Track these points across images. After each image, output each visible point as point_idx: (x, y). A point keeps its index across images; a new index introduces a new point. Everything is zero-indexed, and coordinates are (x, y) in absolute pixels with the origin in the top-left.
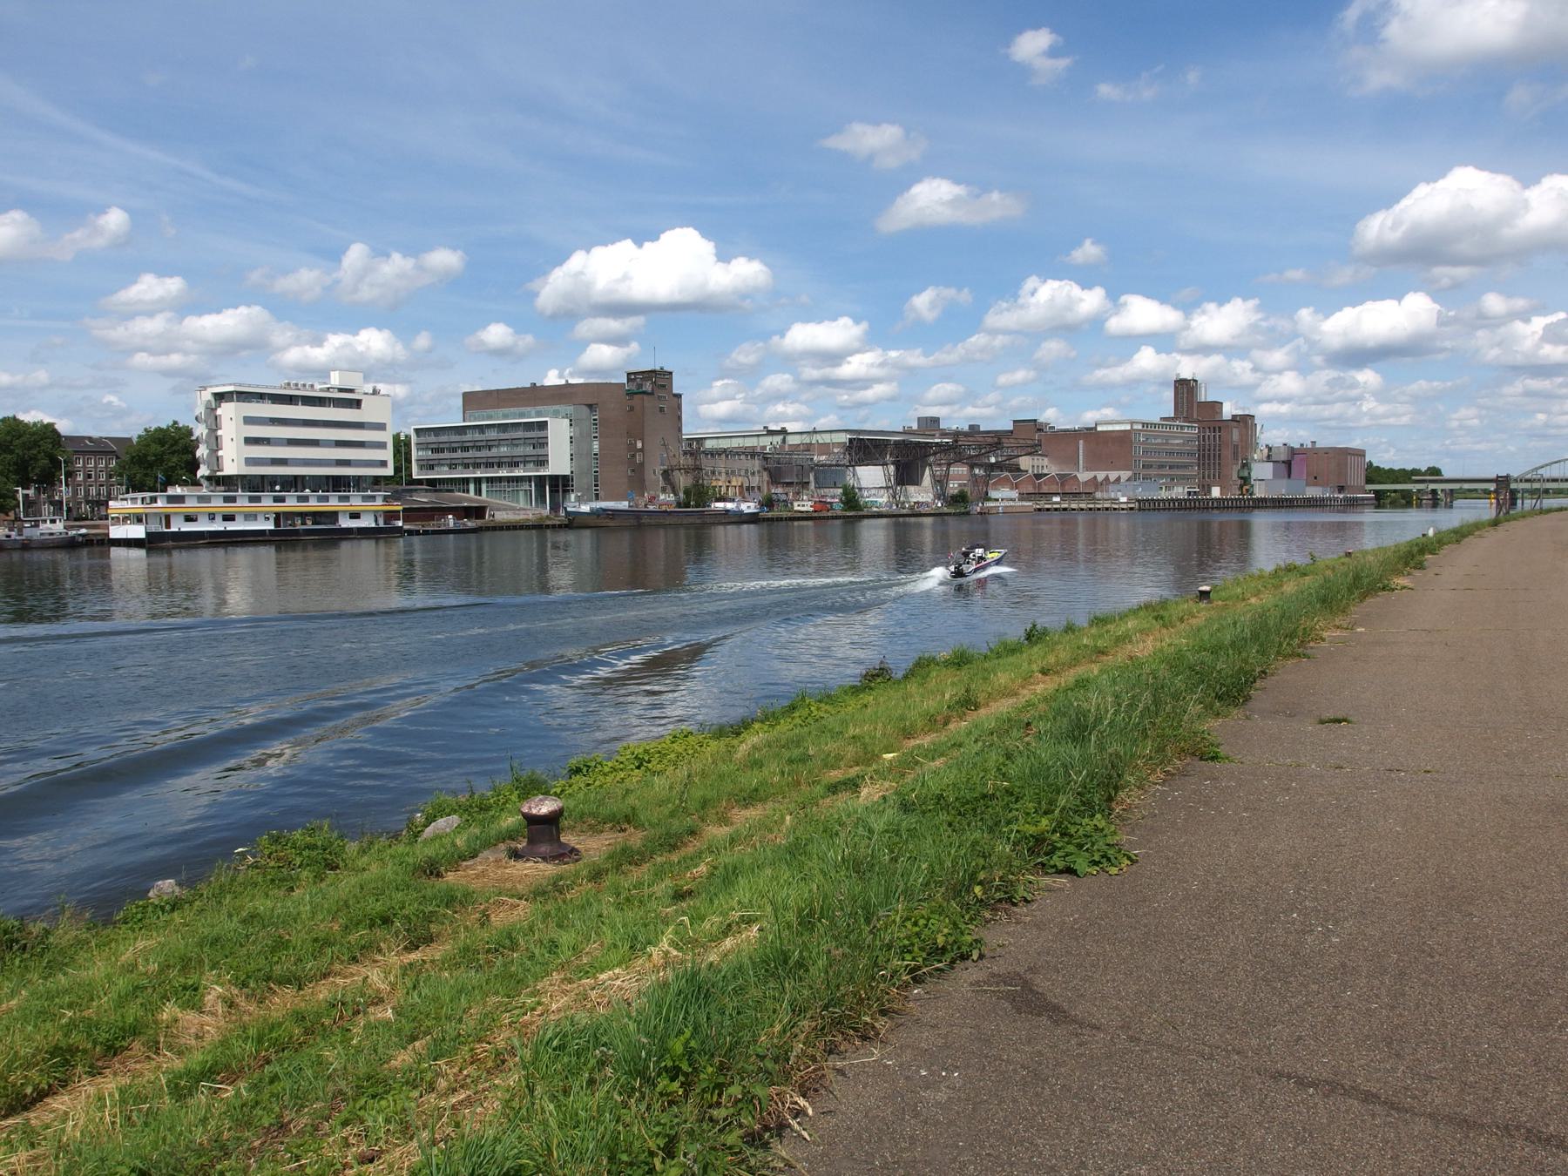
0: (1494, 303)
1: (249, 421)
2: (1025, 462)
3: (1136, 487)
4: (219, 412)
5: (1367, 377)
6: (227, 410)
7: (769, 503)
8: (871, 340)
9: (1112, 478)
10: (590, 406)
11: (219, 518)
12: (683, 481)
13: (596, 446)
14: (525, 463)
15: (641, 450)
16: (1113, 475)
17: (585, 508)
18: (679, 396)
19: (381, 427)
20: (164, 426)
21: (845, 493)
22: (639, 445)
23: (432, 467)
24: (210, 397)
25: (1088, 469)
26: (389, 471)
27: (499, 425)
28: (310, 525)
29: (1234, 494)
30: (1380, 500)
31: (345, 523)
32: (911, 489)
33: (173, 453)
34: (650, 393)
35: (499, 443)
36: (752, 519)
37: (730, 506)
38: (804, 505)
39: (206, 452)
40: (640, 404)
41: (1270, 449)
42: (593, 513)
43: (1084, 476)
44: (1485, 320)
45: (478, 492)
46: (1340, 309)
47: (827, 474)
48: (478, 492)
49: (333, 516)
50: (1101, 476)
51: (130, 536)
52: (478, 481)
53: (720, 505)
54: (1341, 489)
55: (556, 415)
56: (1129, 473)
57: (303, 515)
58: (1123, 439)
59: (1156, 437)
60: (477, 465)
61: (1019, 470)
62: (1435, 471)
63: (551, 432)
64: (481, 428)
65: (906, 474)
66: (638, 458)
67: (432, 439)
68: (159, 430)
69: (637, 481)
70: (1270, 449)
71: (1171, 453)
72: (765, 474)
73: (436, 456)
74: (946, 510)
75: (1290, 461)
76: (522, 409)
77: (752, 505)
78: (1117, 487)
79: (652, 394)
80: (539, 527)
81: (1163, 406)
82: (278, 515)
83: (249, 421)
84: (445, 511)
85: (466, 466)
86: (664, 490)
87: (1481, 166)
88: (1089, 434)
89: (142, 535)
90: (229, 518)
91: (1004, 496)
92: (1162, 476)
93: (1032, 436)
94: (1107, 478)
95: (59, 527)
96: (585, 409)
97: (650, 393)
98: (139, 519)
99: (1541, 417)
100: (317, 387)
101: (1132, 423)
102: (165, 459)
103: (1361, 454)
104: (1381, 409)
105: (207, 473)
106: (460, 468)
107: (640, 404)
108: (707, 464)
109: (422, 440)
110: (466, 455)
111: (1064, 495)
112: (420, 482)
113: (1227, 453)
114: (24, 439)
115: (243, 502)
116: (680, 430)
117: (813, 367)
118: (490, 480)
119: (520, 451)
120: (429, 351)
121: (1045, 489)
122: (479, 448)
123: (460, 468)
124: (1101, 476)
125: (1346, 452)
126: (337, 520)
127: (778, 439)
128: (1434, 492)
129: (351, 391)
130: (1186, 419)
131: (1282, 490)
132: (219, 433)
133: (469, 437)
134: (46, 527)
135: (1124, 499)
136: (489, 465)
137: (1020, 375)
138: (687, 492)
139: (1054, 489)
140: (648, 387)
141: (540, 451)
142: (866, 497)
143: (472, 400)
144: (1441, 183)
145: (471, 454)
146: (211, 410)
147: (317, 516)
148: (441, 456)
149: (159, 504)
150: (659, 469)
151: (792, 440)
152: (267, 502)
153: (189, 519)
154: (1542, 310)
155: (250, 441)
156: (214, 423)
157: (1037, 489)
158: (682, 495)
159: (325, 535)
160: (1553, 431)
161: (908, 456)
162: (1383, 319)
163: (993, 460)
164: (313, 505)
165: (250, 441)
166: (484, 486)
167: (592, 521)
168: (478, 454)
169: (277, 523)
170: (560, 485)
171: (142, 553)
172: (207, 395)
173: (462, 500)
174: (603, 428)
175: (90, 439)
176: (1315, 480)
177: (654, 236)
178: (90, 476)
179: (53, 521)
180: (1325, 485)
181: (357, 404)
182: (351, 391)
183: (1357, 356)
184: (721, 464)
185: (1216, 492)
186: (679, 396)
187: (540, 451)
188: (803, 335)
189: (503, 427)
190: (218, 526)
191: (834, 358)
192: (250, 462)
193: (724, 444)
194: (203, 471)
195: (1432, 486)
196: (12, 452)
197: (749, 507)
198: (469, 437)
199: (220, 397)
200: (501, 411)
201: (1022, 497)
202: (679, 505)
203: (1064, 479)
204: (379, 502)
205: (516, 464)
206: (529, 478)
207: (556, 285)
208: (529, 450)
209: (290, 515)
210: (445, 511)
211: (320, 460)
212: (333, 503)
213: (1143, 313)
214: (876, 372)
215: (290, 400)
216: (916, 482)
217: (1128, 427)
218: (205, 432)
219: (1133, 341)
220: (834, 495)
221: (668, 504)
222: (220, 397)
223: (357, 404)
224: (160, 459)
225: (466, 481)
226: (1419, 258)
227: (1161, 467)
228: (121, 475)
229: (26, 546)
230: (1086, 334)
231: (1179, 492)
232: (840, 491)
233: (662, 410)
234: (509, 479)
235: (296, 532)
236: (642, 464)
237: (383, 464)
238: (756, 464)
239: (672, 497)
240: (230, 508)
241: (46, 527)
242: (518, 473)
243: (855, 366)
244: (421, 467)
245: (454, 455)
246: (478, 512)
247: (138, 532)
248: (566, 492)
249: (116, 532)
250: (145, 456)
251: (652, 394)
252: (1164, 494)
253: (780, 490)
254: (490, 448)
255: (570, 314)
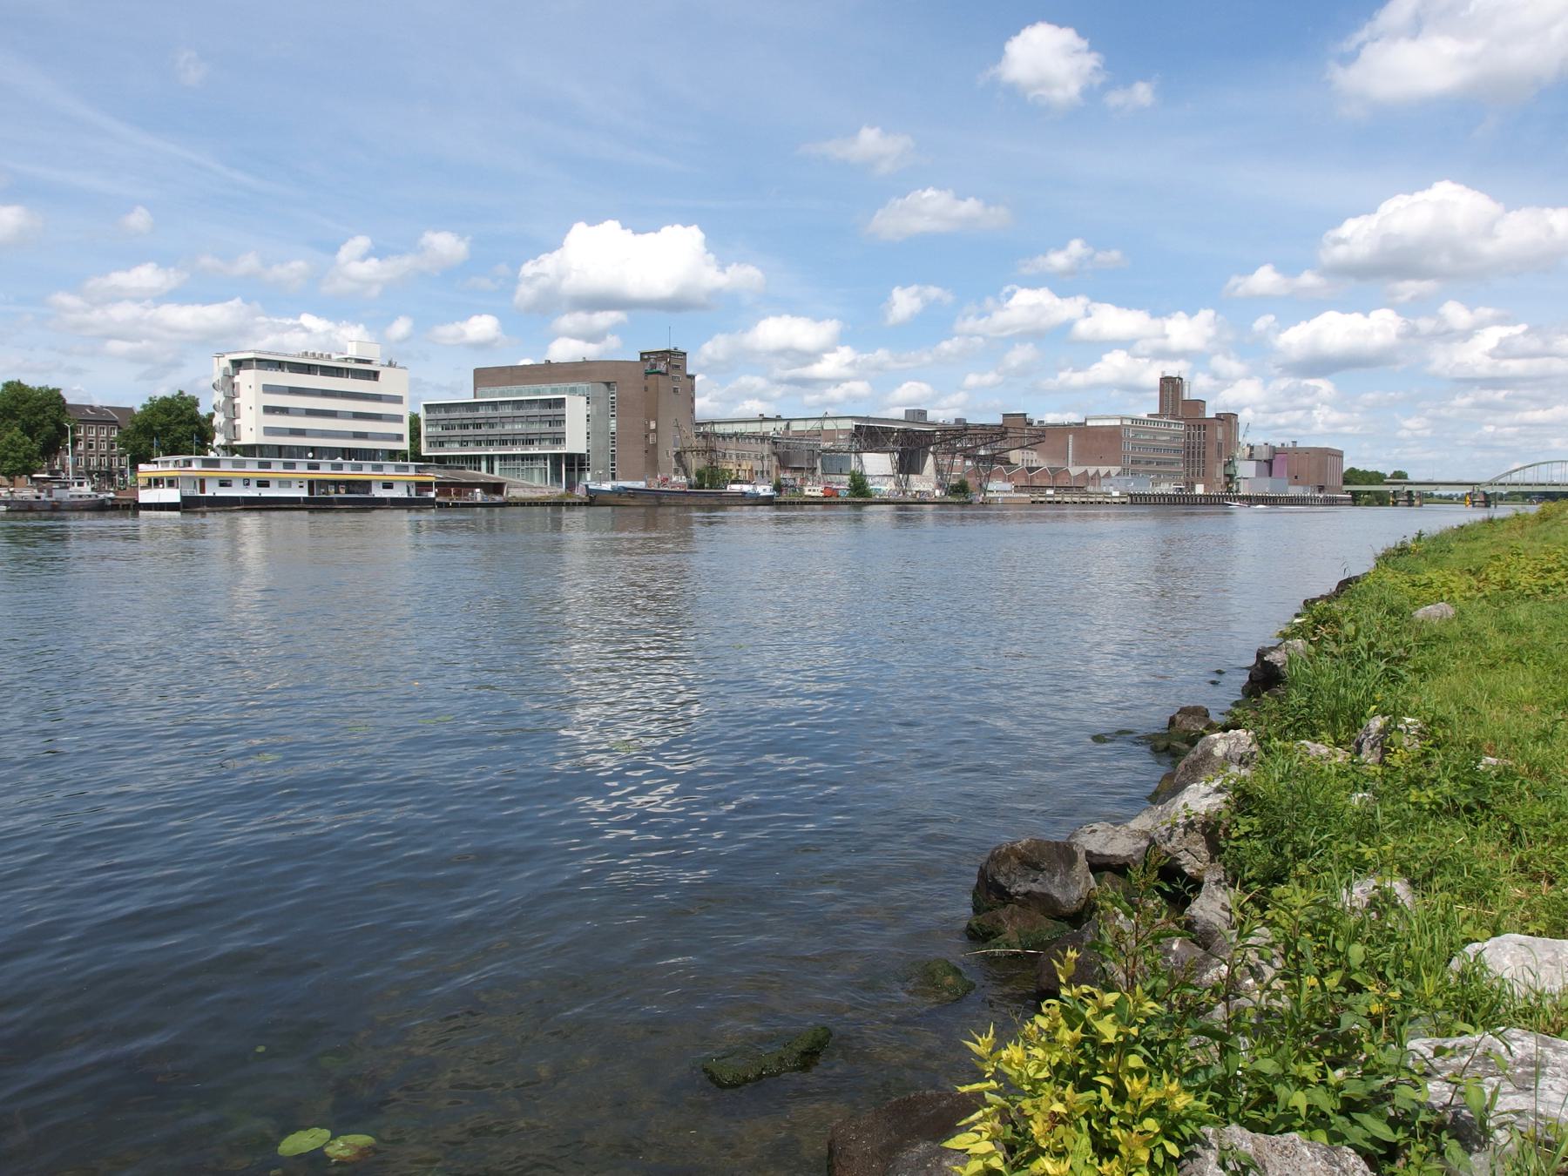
1: (268, 389)
2: (1015, 456)
3: (1128, 482)
4: (237, 379)
5: (1324, 386)
7: (778, 488)
8: (843, 339)
10: (608, 384)
11: (253, 484)
12: (695, 463)
13: (613, 424)
14: (540, 440)
15: (655, 431)
16: (1103, 470)
17: (607, 486)
18: (692, 377)
19: (397, 400)
20: (169, 396)
21: (853, 480)
22: (653, 426)
23: (441, 444)
24: (228, 365)
25: (1076, 464)
26: (405, 445)
28: (343, 494)
29: (1218, 490)
30: (1356, 499)
31: (378, 492)
32: (913, 477)
33: (180, 423)
34: (664, 372)
35: (503, 420)
36: (768, 501)
37: (746, 488)
38: (813, 490)
39: (223, 420)
41: (1252, 448)
42: (614, 491)
43: (1075, 471)
45: (491, 470)
47: (832, 460)
48: (491, 470)
49: (366, 485)
50: (1091, 471)
51: (162, 500)
52: (490, 458)
53: (736, 487)
54: (1321, 489)
55: (573, 391)
56: (1119, 468)
57: (337, 483)
58: (1113, 434)
59: (1145, 433)
60: (490, 443)
62: (1399, 475)
63: (569, 410)
64: (494, 405)
65: (908, 464)
66: (651, 439)
67: (443, 415)
68: (165, 399)
70: (1252, 448)
71: (1156, 449)
72: (774, 459)
73: (446, 433)
74: (949, 499)
75: (1271, 462)
77: (768, 488)
78: (1108, 481)
80: (557, 504)
81: (1148, 406)
82: (311, 483)
83: (268, 389)
84: (472, 486)
85: (479, 443)
86: (676, 472)
88: (1080, 429)
90: (263, 484)
91: (998, 488)
93: (1016, 430)
95: (87, 489)
96: (603, 387)
99: (1491, 429)
100: (335, 356)
102: (175, 427)
103: (1339, 455)
105: (223, 442)
106: (471, 445)
108: (720, 445)
109: (432, 416)
110: (478, 432)
111: (1057, 488)
112: (430, 459)
113: (1211, 451)
114: (30, 404)
115: (277, 467)
116: (693, 411)
117: (787, 361)
118: (503, 458)
119: (535, 428)
121: (1037, 482)
122: (492, 426)
123: (471, 445)
124: (1091, 471)
126: (369, 490)
128: (1410, 493)
129: (369, 362)
130: (1174, 416)
131: (1266, 487)
133: (482, 412)
134: (75, 490)
135: (1116, 494)
137: (990, 378)
138: (700, 475)
139: (1045, 482)
140: (662, 367)
141: (556, 429)
142: (874, 485)
143: (483, 377)
144: (1419, 196)
145: (484, 430)
146: (229, 377)
147: (350, 485)
148: (452, 432)
149: (195, 467)
150: (672, 450)
151: (795, 426)
152: (302, 469)
153: (224, 483)
155: (269, 410)
156: (231, 391)
157: (1030, 481)
158: (694, 477)
159: (358, 499)
160: (1502, 443)
161: (910, 443)
162: (1337, 330)
163: (982, 452)
164: (348, 473)
165: (269, 410)
166: (497, 464)
167: (613, 499)
169: (311, 491)
170: (576, 463)
171: (177, 514)
172: (225, 362)
173: (475, 476)
174: (619, 407)
175: (91, 407)
176: (1296, 479)
179: (80, 484)
180: (1305, 484)
181: (375, 375)
182: (369, 362)
183: (1320, 365)
185: (1200, 489)
186: (692, 377)
187: (556, 429)
188: (775, 331)
189: (518, 404)
190: (253, 492)
192: (269, 431)
193: (738, 428)
194: (219, 439)
197: (764, 490)
198: (482, 412)
199: (238, 364)
200: (514, 388)
201: (1018, 489)
202: (691, 487)
203: (1056, 472)
204: (412, 472)
205: (531, 442)
206: (545, 457)
207: (541, 269)
208: (545, 428)
209: (324, 483)
210: (472, 486)
211: (340, 430)
212: (367, 472)
213: (1113, 320)
214: (847, 372)
215: (308, 369)
217: (1118, 423)
218: (222, 399)
219: (1100, 347)
220: (843, 483)
222: (238, 364)
223: (375, 375)
224: (166, 429)
225: (477, 459)
226: (1390, 268)
227: (1149, 463)
228: (124, 445)
229: (56, 507)
230: (1055, 340)
231: (1167, 488)
233: (675, 390)
234: (524, 457)
236: (655, 446)
237: (400, 438)
238: (766, 448)
239: (684, 480)
240: (264, 474)
242: (532, 450)
243: (828, 366)
244: (430, 444)
245: (465, 432)
246: (497, 488)
247: (172, 495)
248: (581, 470)
249: (146, 496)
250: (150, 425)
253: (788, 475)
254: (503, 424)
255: (551, 304)
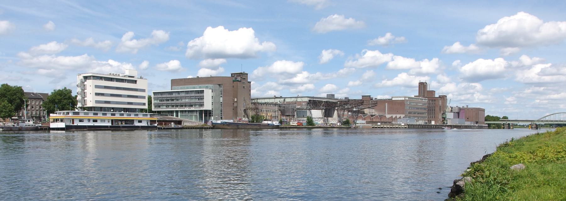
0: (526, 60)
1: (97, 87)
2: (366, 111)
4: (85, 83)
5: (478, 86)
6: (89, 83)
7: (281, 122)
8: (304, 69)
9: (398, 117)
10: (219, 85)
11: (91, 121)
12: (251, 113)
13: (221, 99)
14: (195, 105)
15: (236, 102)
16: (398, 116)
17: (219, 122)
19: (143, 91)
20: (61, 89)
21: (308, 119)
22: (236, 100)
23: (159, 106)
24: (82, 78)
25: (389, 114)
27: (184, 92)
28: (124, 125)
29: (439, 123)
30: (489, 126)
31: (137, 124)
32: (329, 119)
33: (65, 99)
34: (240, 81)
35: (182, 98)
36: (277, 127)
37: (269, 122)
40: (236, 84)
41: (452, 108)
42: (222, 124)
43: (388, 116)
44: (523, 67)
45: (177, 116)
46: (468, 63)
47: (300, 112)
48: (177, 116)
49: (132, 121)
50: (394, 116)
52: (177, 112)
53: (266, 122)
54: (477, 123)
55: (207, 87)
56: (404, 115)
57: (121, 121)
59: (413, 103)
60: (177, 106)
61: (364, 113)
63: (205, 94)
64: (178, 92)
65: (328, 114)
66: (235, 105)
67: (160, 96)
68: (60, 90)
69: (235, 113)
70: (452, 108)
71: (417, 108)
73: (161, 102)
74: (343, 126)
75: (459, 113)
76: (194, 86)
77: (277, 122)
79: (240, 81)
80: (201, 128)
81: (415, 93)
82: (112, 121)
83: (97, 87)
85: (173, 106)
86: (244, 116)
87: (525, 12)
89: (64, 127)
90: (95, 121)
91: (360, 122)
92: (415, 117)
94: (396, 117)
95: (31, 123)
97: (240, 81)
98: (62, 121)
99: (538, 101)
100: (121, 75)
101: (405, 97)
102: (63, 100)
103: (483, 110)
104: (482, 97)
105: (81, 106)
107: (236, 84)
108: (260, 107)
109: (156, 96)
110: (172, 102)
111: (382, 122)
112: (155, 112)
113: (437, 109)
115: (100, 115)
116: (250, 95)
117: (284, 77)
118: (182, 111)
119: (193, 101)
120: (146, 69)
121: (374, 120)
122: (178, 100)
124: (394, 116)
125: (479, 110)
126: (133, 123)
127: (282, 100)
128: (509, 124)
129: (133, 77)
130: (424, 96)
131: (457, 122)
132: (85, 91)
135: (403, 124)
136: (182, 106)
138: (253, 117)
139: (378, 120)
140: (239, 79)
141: (201, 101)
142: (315, 121)
144: (512, 17)
145: (175, 102)
146: (83, 83)
147: (126, 121)
148: (163, 102)
149: (70, 115)
150: (243, 109)
151: (287, 100)
152: (109, 116)
153: (81, 121)
154: (542, 62)
155: (97, 94)
156: (84, 88)
157: (372, 120)
158: (250, 119)
159: (129, 126)
160: (542, 106)
161: (329, 106)
162: (483, 65)
163: (355, 110)
164: (125, 117)
165: (97, 94)
166: (179, 114)
167: (221, 126)
168: (177, 102)
169: (112, 123)
170: (208, 113)
171: (64, 132)
172: (81, 77)
174: (223, 93)
175: (33, 93)
176: (468, 119)
177: (232, 30)
178: (33, 107)
181: (135, 82)
182: (133, 77)
183: (476, 78)
184: (264, 108)
185: (433, 123)
186: (250, 82)
187: (201, 101)
190: (91, 124)
191: (293, 75)
192: (97, 102)
193: (266, 101)
194: (79, 105)
195: (508, 122)
196: (6, 97)
197: (276, 123)
198: (174, 95)
199: (86, 78)
200: (186, 86)
201: (368, 123)
203: (381, 117)
204: (149, 116)
205: (192, 106)
206: (197, 111)
207: (195, 44)
208: (197, 101)
209: (117, 121)
211: (122, 102)
212: (132, 117)
213: (402, 62)
214: (306, 81)
216: (331, 116)
217: (404, 99)
218: (80, 90)
219: (397, 71)
220: (304, 121)
221: (245, 121)
222: (86, 78)
223: (135, 82)
224: (60, 101)
225: (172, 112)
226: (502, 43)
227: (415, 113)
230: (381, 69)
231: (421, 122)
232: (305, 119)
233: (244, 87)
234: (189, 111)
235: (119, 127)
236: (237, 107)
237: (144, 104)
238: (276, 108)
239: (247, 119)
240: (95, 117)
241: (27, 123)
243: (299, 78)
244: (155, 107)
245: (168, 102)
246: (179, 122)
247: (62, 125)
248: (210, 116)
249: (53, 125)
250: (54, 100)
251: (240, 81)
252: (418, 123)
253: (284, 118)
255: (199, 56)
